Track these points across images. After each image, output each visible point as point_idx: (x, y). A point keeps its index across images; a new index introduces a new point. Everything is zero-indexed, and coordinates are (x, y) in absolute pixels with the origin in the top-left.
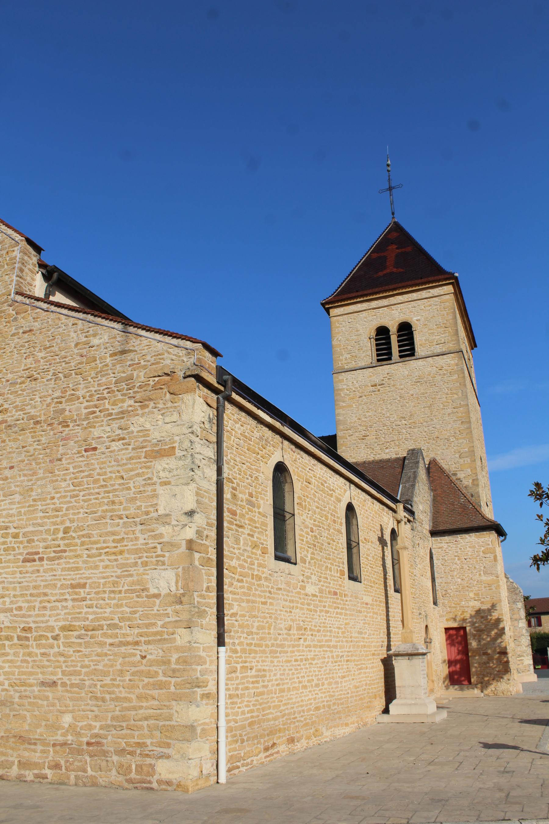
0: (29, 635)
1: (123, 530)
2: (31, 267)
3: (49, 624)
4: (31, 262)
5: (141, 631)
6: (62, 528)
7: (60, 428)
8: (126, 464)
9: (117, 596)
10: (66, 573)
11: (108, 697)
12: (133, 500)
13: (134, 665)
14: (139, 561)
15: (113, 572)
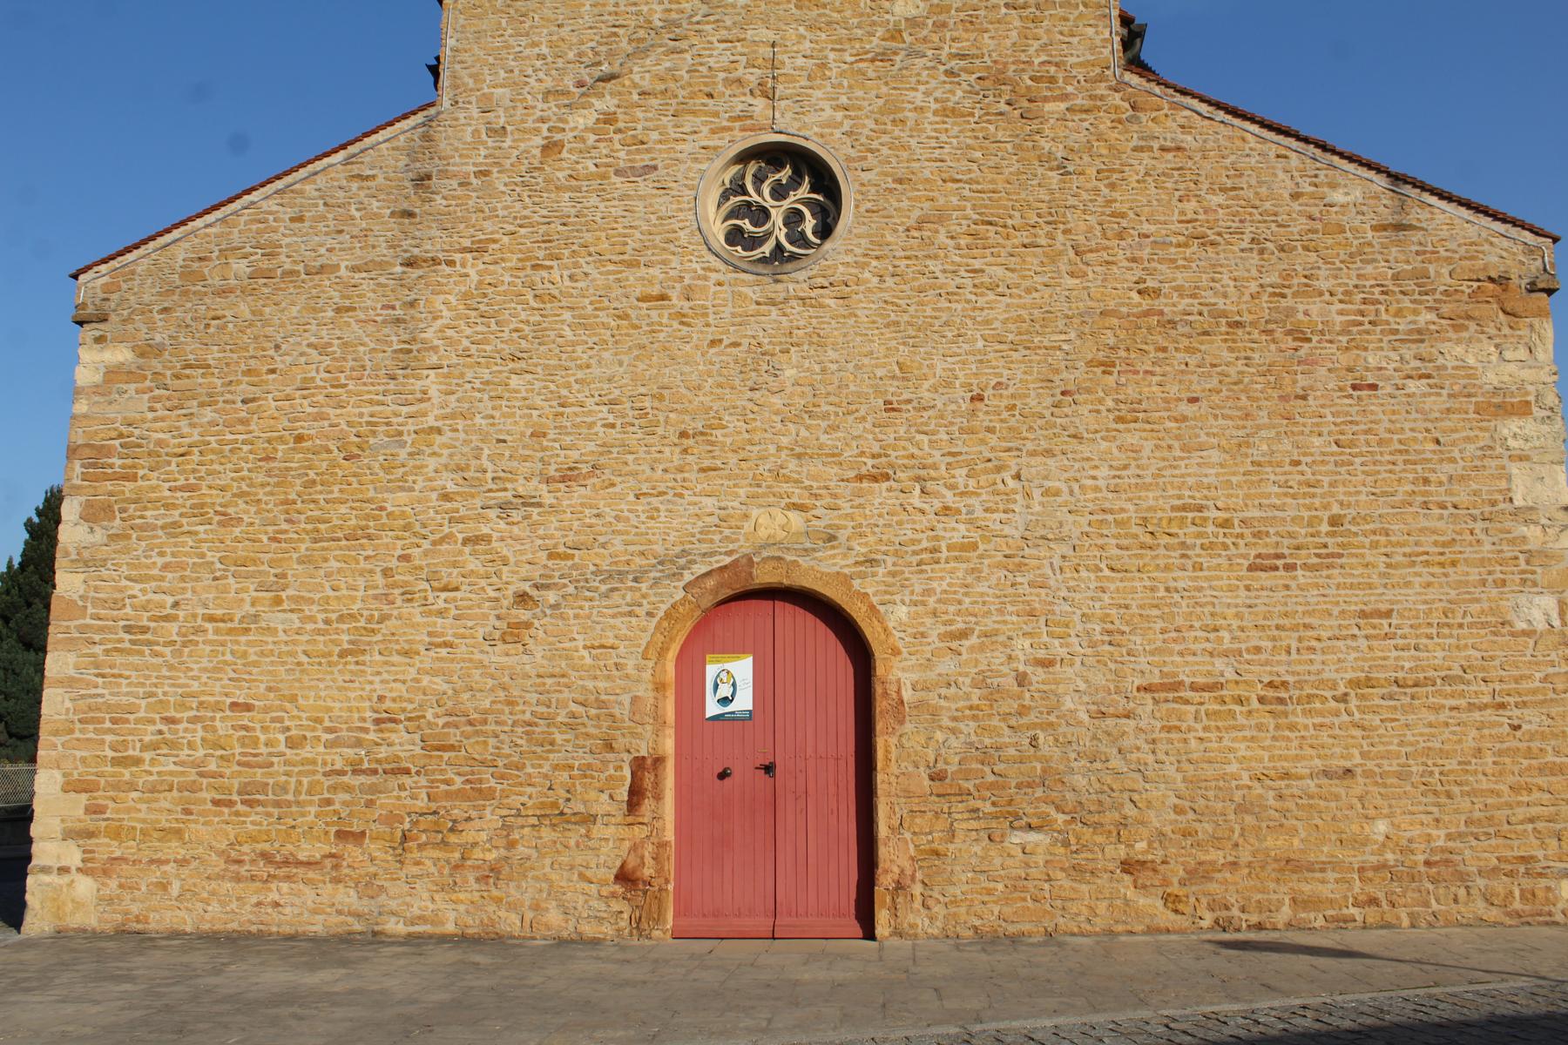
6: (1325, 515)
11: (1456, 790)
14: (1490, 578)
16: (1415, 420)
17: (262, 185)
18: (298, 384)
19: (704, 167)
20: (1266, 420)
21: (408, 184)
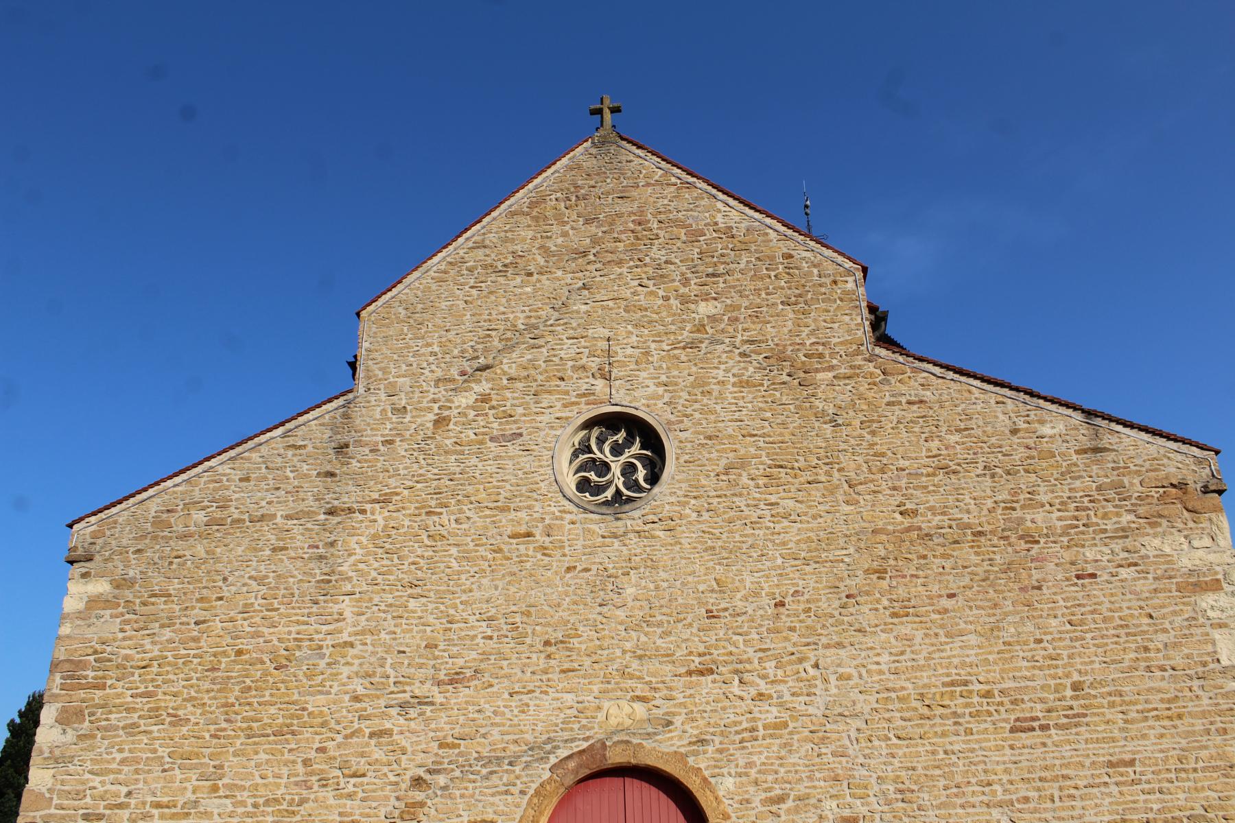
6: (1068, 682)
14: (1213, 728)
16: (1130, 600)
17: (219, 454)
18: (240, 609)
19: (558, 433)
20: (1011, 608)
21: (331, 451)
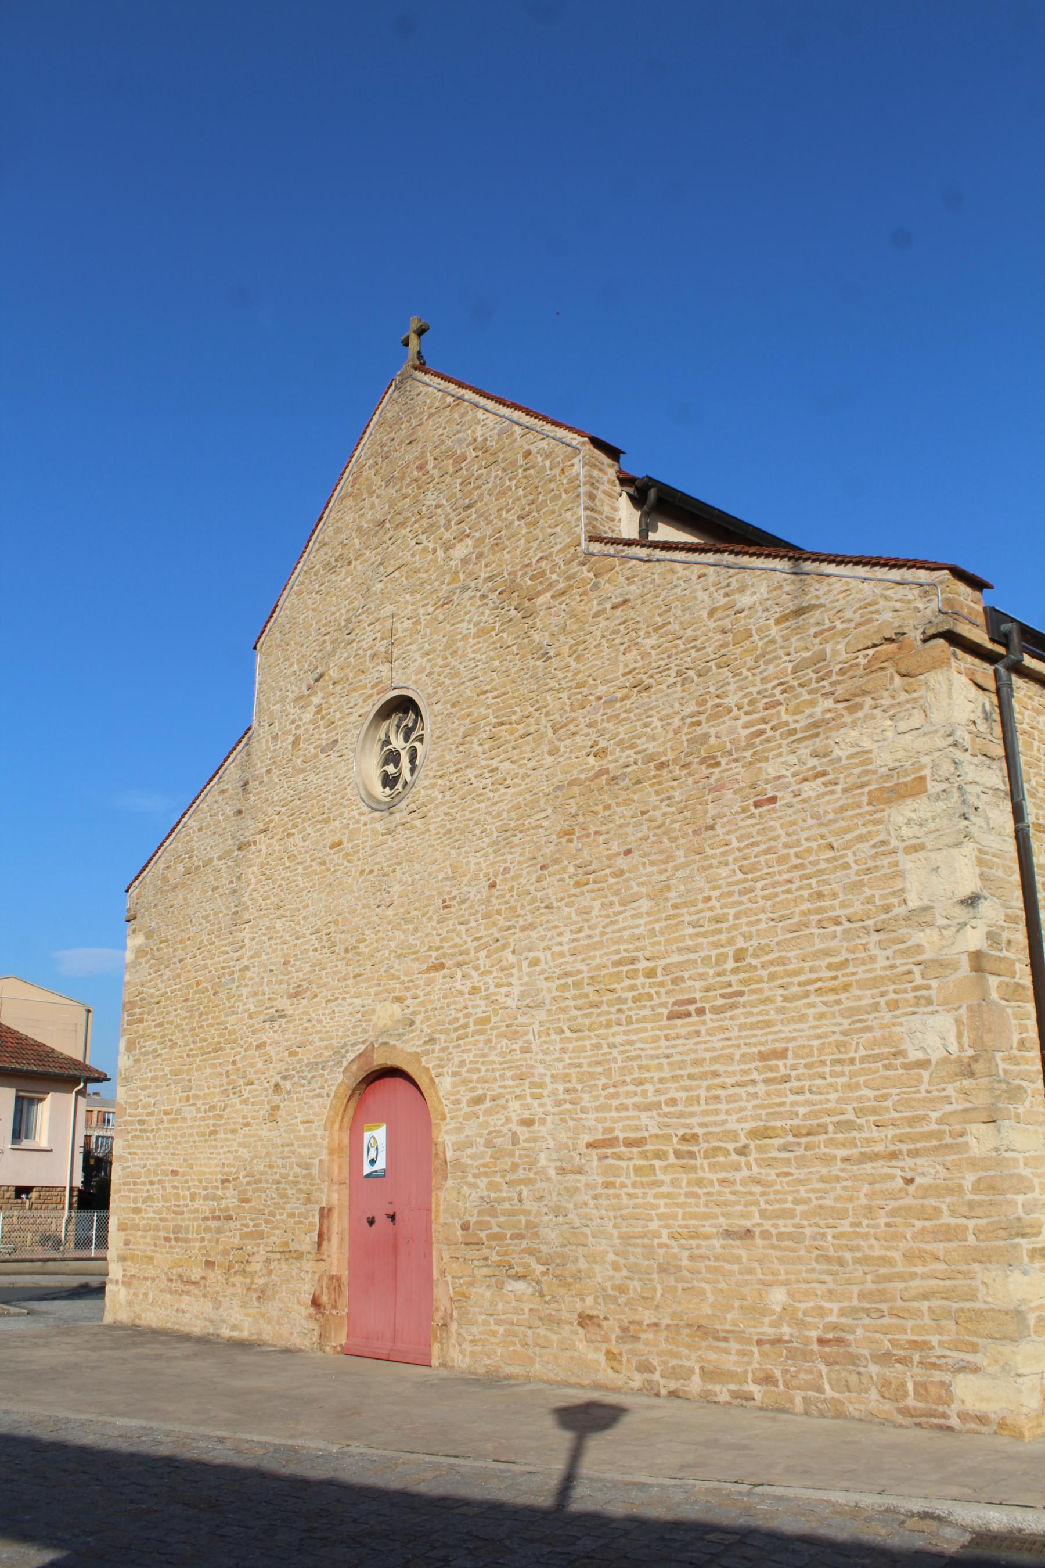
0: (695, 1149)
1: (845, 944)
2: (607, 487)
3: (728, 1126)
4: (605, 478)
5: (898, 1131)
6: (730, 951)
7: (704, 770)
8: (835, 821)
9: (847, 1069)
10: (749, 1032)
11: (848, 1256)
12: (855, 887)
13: (892, 1196)
14: (882, 1001)
15: (836, 1024)
